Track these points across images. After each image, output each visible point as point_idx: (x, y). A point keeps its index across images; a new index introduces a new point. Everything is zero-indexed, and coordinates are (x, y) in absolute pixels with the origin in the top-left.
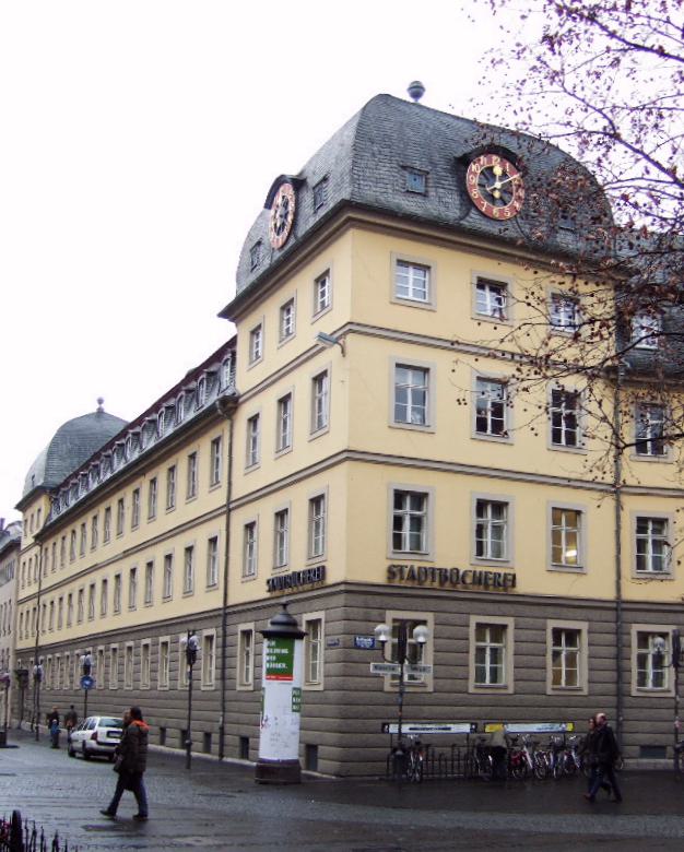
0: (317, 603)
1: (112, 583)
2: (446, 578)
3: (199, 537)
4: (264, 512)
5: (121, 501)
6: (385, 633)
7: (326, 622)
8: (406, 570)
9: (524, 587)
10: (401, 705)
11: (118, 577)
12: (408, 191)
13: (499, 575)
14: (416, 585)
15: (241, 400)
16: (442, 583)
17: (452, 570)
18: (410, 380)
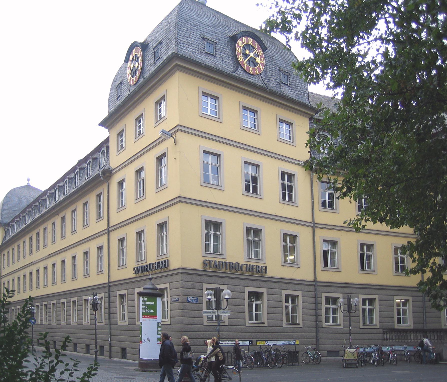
1: (22, 278)
3: (92, 247)
4: (130, 233)
5: (45, 229)
7: (128, 295)
8: (213, 263)
9: (271, 273)
10: (219, 332)
11: (45, 268)
12: (206, 53)
13: (259, 267)
14: (216, 270)
15: (113, 172)
18: (211, 160)
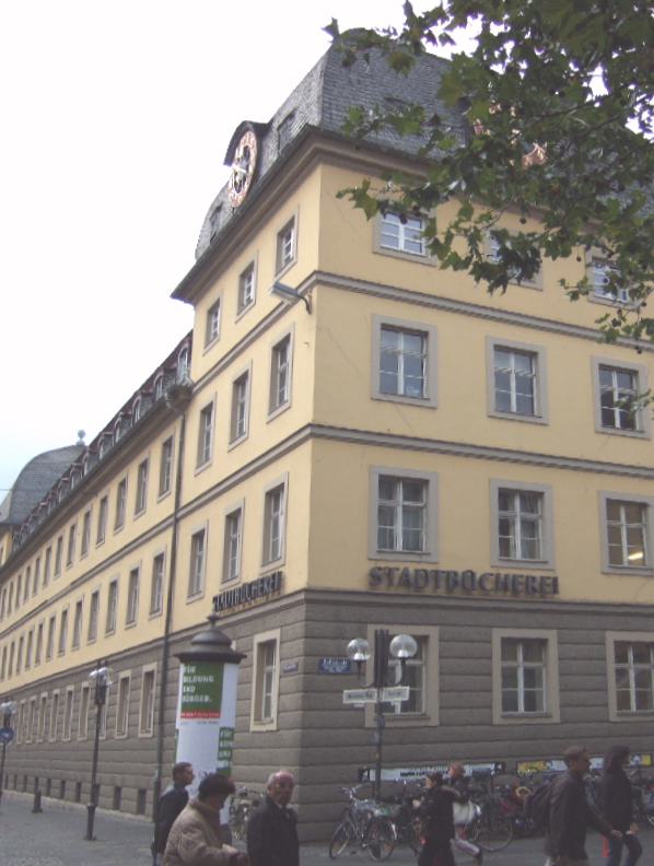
0: (271, 620)
2: (456, 583)
3: (144, 557)
4: (212, 520)
6: (364, 651)
7: (281, 643)
8: (397, 575)
13: (534, 578)
15: (195, 389)
16: (449, 589)
17: (464, 573)
